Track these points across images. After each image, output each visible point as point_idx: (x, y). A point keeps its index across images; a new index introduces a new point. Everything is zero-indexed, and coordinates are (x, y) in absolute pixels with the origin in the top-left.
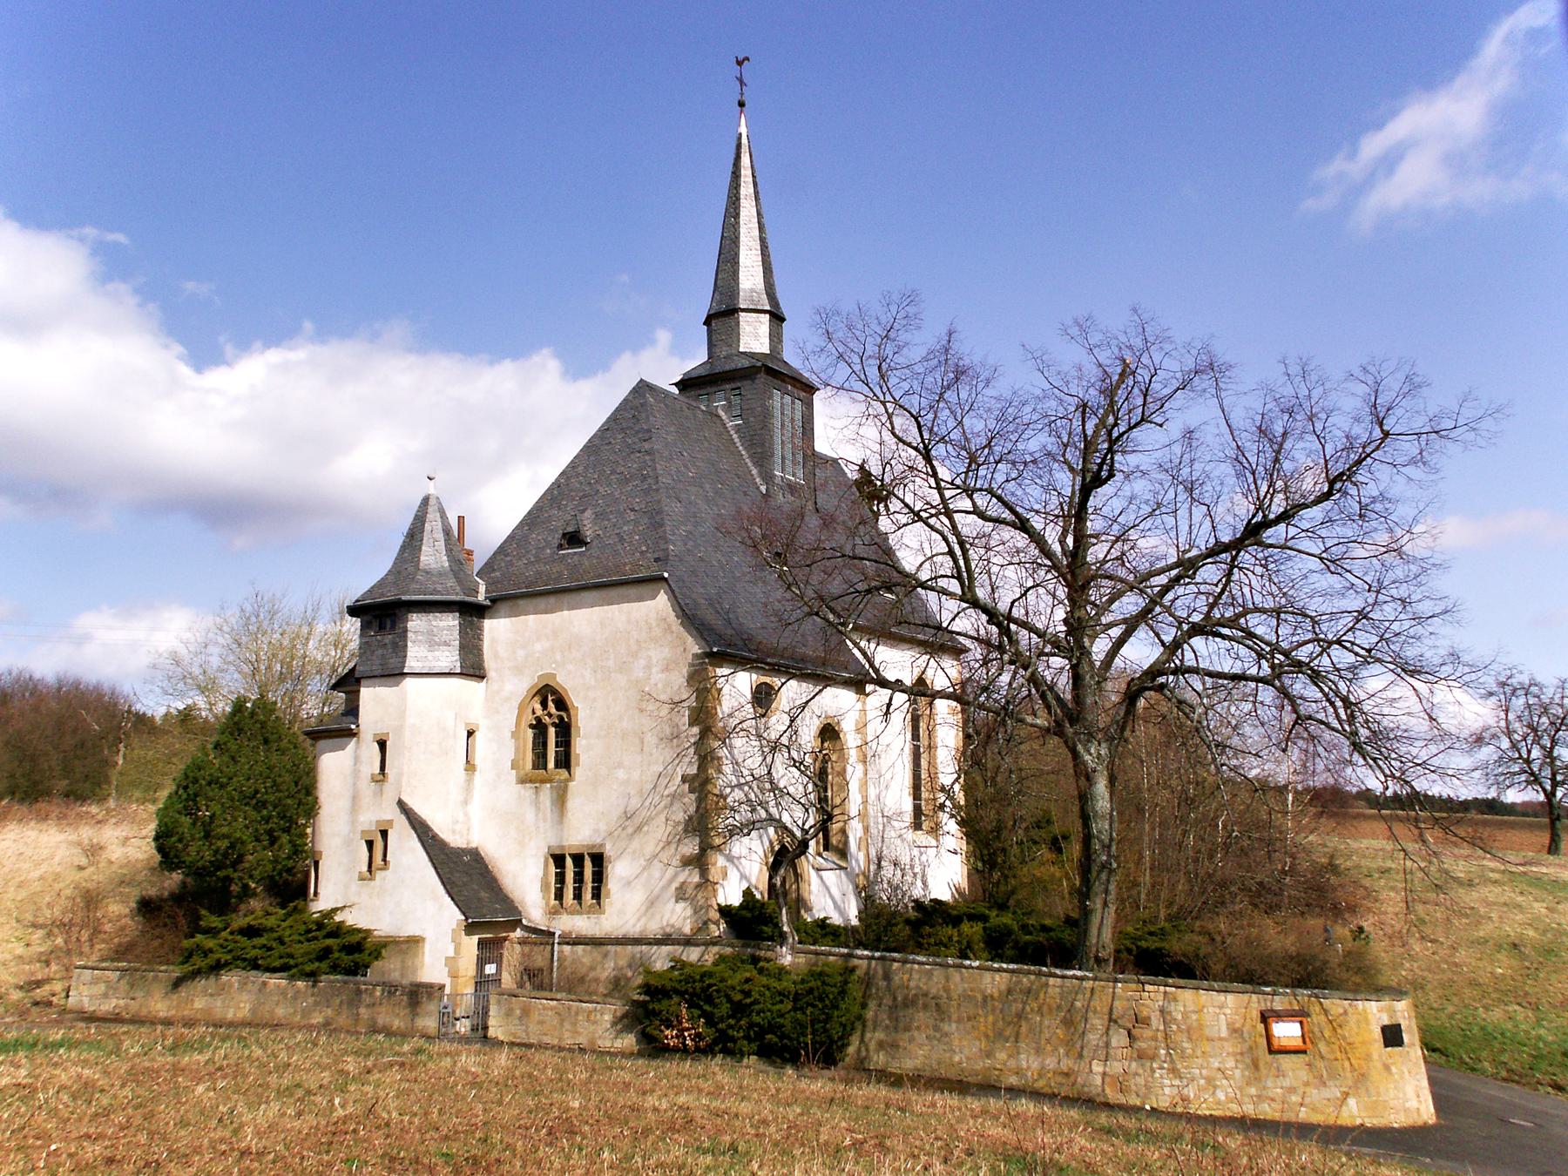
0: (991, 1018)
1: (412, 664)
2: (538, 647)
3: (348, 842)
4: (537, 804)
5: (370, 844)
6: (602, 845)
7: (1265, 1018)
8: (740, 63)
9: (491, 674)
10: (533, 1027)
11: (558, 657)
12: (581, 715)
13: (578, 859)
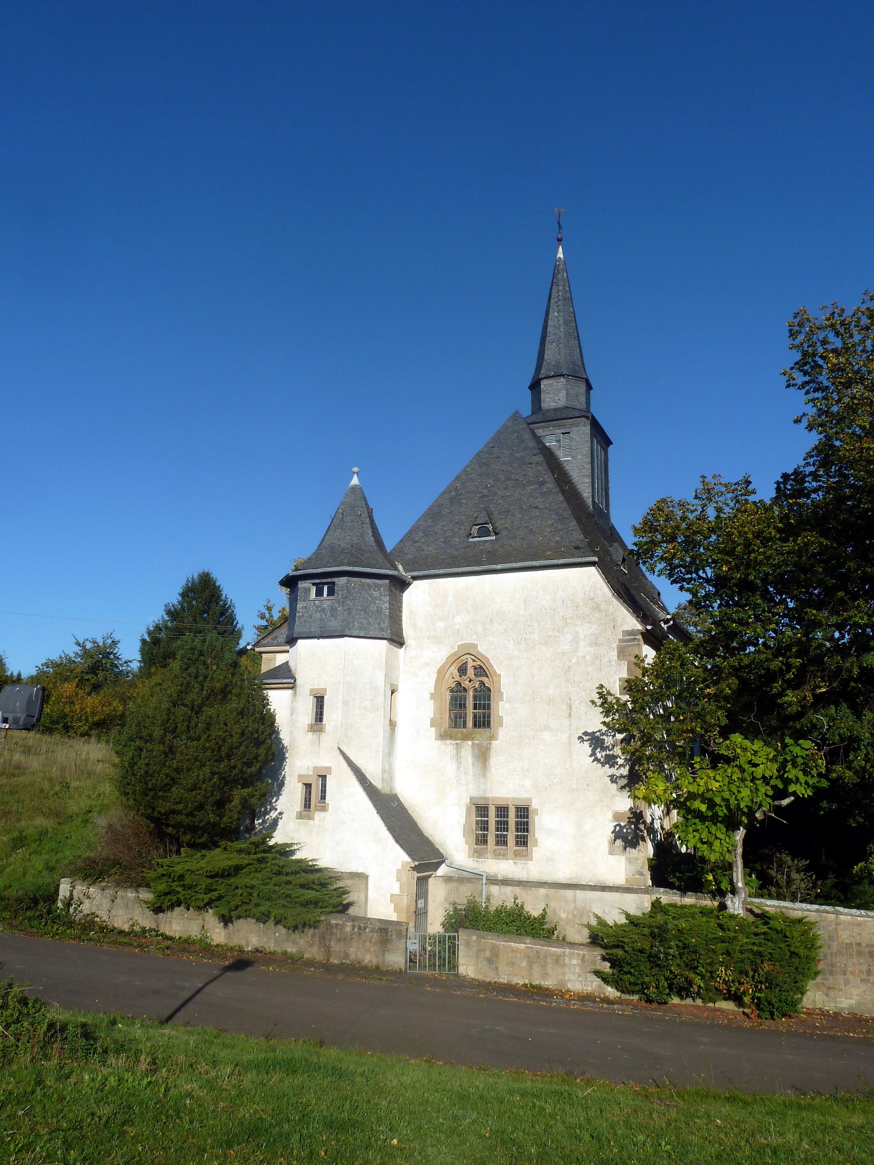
2: (458, 620)
4: (458, 757)
5: (308, 786)
6: (530, 799)
10: (503, 968)
11: (480, 629)
13: (502, 811)
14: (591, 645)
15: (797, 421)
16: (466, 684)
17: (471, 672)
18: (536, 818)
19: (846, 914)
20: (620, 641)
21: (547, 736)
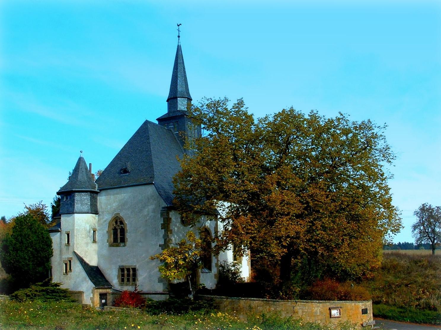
1: (76, 209)
3: (59, 264)
5: (66, 264)
7: (330, 309)
8: (178, 26)
9: (100, 213)
12: (128, 226)
13: (128, 270)
14: (153, 212)
15: (275, 113)
16: (117, 227)
17: (118, 223)
18: (138, 272)
19: (230, 299)
20: (161, 211)
21: (140, 244)
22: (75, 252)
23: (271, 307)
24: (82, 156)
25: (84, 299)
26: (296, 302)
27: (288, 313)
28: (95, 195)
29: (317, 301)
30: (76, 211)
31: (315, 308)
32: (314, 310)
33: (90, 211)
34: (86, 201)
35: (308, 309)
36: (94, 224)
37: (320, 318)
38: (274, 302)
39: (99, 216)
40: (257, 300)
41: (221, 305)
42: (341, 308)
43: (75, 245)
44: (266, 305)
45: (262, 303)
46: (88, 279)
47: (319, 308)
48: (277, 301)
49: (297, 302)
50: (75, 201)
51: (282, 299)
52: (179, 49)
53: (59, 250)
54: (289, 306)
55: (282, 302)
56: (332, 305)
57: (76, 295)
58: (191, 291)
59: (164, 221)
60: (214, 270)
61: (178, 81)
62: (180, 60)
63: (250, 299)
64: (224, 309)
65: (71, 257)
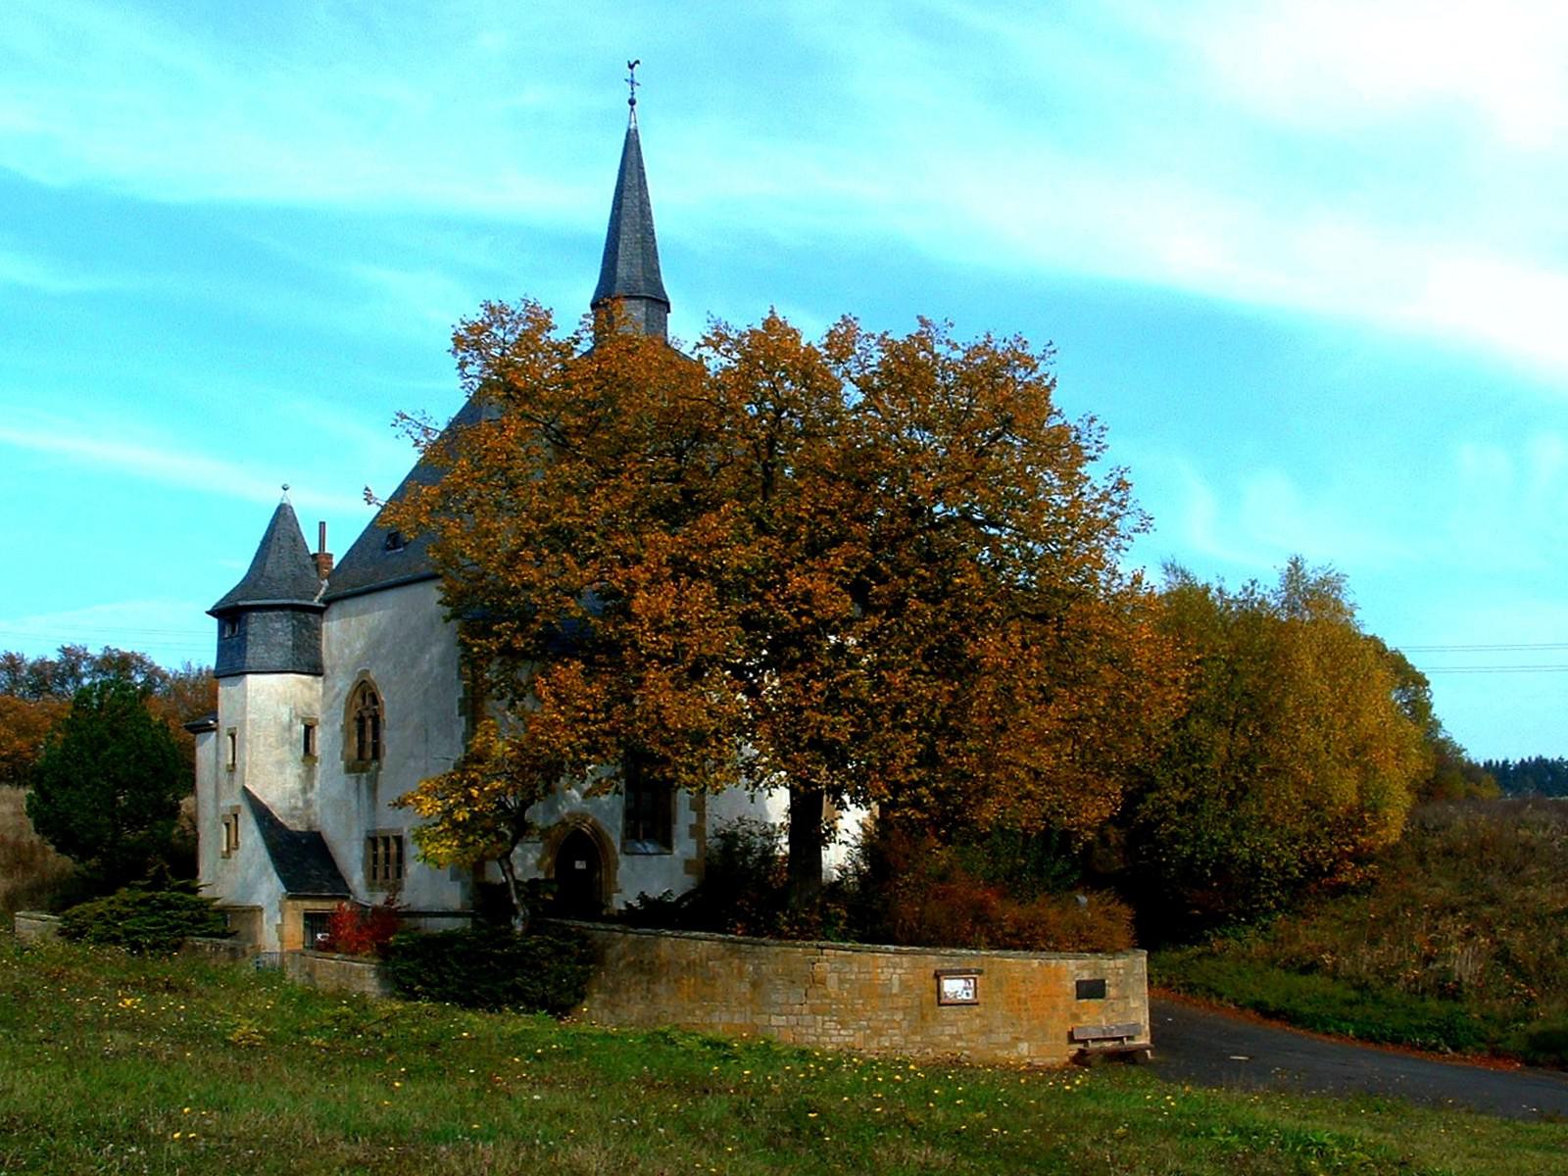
0: (693, 981)
1: (250, 662)
3: (215, 826)
5: (227, 825)
7: (937, 976)
8: (631, 67)
9: (328, 671)
13: (386, 840)
16: (366, 714)
22: (245, 790)
23: (745, 963)
24: (285, 501)
25: (261, 928)
26: (818, 947)
27: (793, 982)
28: (312, 617)
29: (892, 948)
30: (250, 667)
31: (885, 970)
32: (882, 977)
33: (290, 664)
34: (280, 637)
35: (860, 972)
36: (309, 706)
37: (900, 1002)
38: (754, 944)
39: (324, 680)
40: (706, 939)
41: (609, 951)
42: (979, 972)
43: (247, 770)
44: (730, 955)
45: (721, 947)
46: (271, 869)
47: (899, 971)
48: (763, 944)
49: (822, 948)
50: (249, 637)
51: (780, 935)
52: (632, 145)
53: (213, 785)
54: (798, 961)
55: (778, 945)
56: (948, 961)
57: (245, 915)
58: (515, 906)
59: (465, 692)
60: (685, 847)
61: (621, 246)
62: (632, 179)
63: (686, 934)
64: (617, 966)
65: (237, 803)
